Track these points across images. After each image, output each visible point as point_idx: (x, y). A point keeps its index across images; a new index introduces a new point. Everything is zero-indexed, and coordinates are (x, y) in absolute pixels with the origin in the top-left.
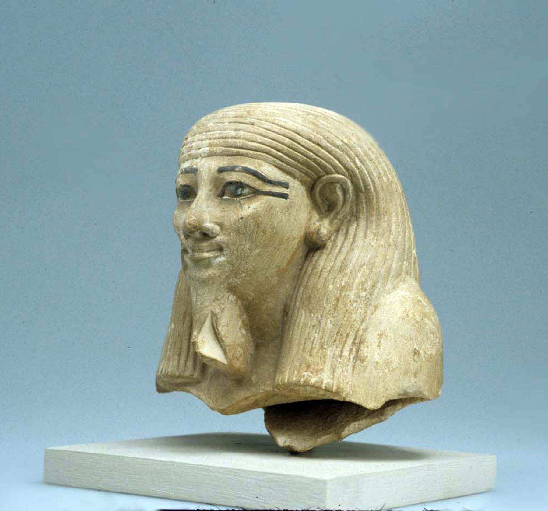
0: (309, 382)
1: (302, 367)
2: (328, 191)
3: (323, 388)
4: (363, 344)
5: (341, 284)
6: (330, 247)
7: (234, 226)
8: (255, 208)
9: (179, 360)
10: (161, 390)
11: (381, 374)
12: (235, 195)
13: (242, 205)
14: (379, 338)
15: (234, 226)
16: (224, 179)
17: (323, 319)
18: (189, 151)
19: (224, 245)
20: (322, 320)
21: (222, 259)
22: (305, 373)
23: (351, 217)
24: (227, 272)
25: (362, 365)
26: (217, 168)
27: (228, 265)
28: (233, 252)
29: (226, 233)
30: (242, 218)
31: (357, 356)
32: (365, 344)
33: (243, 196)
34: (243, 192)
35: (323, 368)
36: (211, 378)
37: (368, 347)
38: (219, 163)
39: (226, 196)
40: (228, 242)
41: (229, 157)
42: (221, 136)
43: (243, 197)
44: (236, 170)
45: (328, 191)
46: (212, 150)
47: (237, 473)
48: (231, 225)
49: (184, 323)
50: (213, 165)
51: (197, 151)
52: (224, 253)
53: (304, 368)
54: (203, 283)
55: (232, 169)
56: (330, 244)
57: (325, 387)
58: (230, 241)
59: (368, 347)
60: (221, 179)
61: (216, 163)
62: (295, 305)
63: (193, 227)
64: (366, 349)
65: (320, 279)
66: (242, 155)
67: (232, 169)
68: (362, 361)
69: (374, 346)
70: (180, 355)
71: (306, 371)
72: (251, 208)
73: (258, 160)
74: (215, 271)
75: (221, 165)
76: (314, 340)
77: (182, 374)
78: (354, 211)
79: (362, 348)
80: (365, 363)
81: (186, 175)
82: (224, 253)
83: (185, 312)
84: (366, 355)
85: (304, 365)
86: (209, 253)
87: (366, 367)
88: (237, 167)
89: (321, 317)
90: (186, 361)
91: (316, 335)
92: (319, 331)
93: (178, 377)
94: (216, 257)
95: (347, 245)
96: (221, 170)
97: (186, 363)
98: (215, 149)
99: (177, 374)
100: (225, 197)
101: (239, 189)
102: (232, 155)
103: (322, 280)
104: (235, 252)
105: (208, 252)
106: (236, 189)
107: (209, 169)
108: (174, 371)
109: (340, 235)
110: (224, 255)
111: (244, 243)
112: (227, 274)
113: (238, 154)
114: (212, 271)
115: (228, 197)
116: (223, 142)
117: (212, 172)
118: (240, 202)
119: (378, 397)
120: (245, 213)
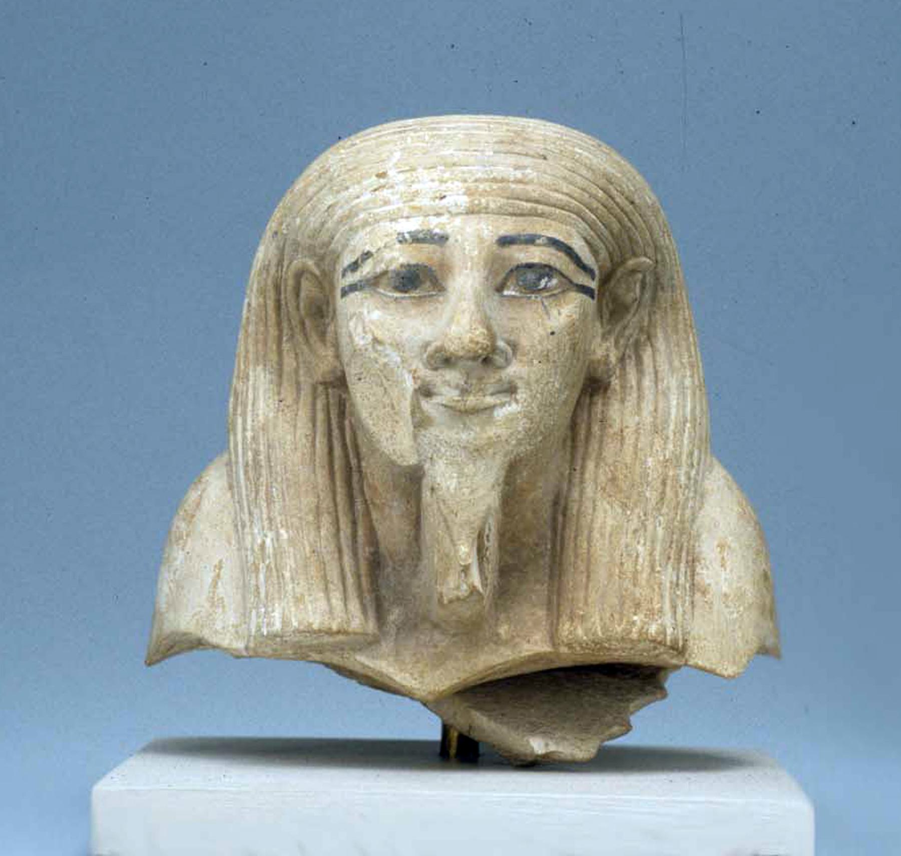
0: (647, 633)
1: (626, 606)
2: (624, 286)
3: (668, 643)
4: (699, 561)
5: (665, 456)
6: (618, 388)
7: (539, 347)
8: (569, 314)
9: (328, 600)
10: (150, 663)
11: (735, 615)
12: (532, 289)
13: (549, 308)
14: (720, 552)
15: (539, 347)
16: (510, 258)
17: (649, 517)
18: (412, 200)
19: (520, 384)
20: (647, 520)
21: (514, 408)
22: (635, 618)
23: (638, 334)
24: (519, 432)
25: (706, 600)
26: (496, 238)
27: (525, 420)
28: (535, 396)
29: (525, 359)
30: (553, 333)
31: (693, 585)
32: (703, 562)
33: (547, 292)
34: (549, 284)
35: (662, 608)
36: (397, 634)
37: (708, 568)
38: (497, 228)
39: (508, 290)
40: (529, 377)
41: (514, 218)
42: (492, 176)
43: (547, 294)
44: (538, 241)
45: (624, 286)
46: (476, 202)
47: (609, 805)
48: (533, 346)
49: (319, 528)
50: (486, 232)
51: (437, 201)
52: (518, 397)
53: (630, 607)
54: (475, 454)
55: (531, 240)
56: (617, 381)
57: (381, 645)
58: (532, 375)
59: (708, 568)
60: (504, 259)
61: (490, 228)
62: (582, 493)
63: (482, 348)
64: (705, 572)
65: (625, 447)
66: (542, 215)
67: (531, 240)
68: (704, 593)
69: (717, 565)
70: (326, 590)
71: (635, 614)
72: (563, 315)
73: (566, 225)
74: (499, 432)
75: (502, 232)
76: (637, 557)
77: (345, 626)
78: (646, 324)
79: (698, 570)
80: (707, 596)
81: (414, 245)
82: (518, 397)
83: (318, 507)
84: (708, 581)
85: (629, 603)
86: (494, 397)
87: (712, 603)
88: (539, 237)
89: (645, 515)
90: (345, 599)
91: (640, 548)
92: (645, 540)
93: (338, 632)
94: (503, 405)
95: (647, 382)
96: (505, 241)
97: (346, 605)
98: (483, 201)
99: (335, 627)
100: (506, 293)
101: (544, 278)
102: (522, 215)
103: (629, 449)
104: (538, 395)
105: (492, 394)
106: (539, 279)
107: (481, 240)
108: (326, 623)
109: (628, 369)
110: (517, 401)
111: (552, 380)
112: (519, 436)
113: (534, 213)
114: (494, 431)
115: (513, 293)
116: (499, 188)
117: (487, 244)
118: (543, 303)
119: (737, 658)
120: (557, 324)
